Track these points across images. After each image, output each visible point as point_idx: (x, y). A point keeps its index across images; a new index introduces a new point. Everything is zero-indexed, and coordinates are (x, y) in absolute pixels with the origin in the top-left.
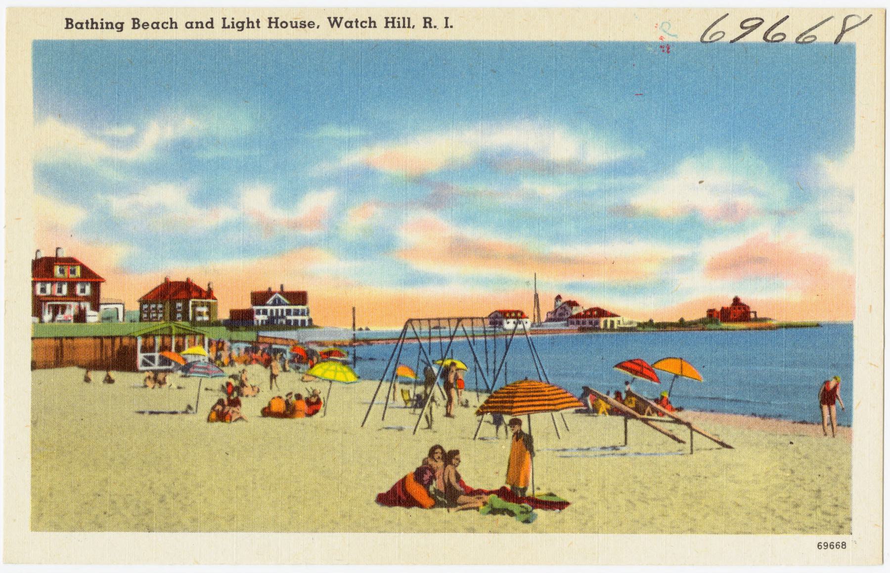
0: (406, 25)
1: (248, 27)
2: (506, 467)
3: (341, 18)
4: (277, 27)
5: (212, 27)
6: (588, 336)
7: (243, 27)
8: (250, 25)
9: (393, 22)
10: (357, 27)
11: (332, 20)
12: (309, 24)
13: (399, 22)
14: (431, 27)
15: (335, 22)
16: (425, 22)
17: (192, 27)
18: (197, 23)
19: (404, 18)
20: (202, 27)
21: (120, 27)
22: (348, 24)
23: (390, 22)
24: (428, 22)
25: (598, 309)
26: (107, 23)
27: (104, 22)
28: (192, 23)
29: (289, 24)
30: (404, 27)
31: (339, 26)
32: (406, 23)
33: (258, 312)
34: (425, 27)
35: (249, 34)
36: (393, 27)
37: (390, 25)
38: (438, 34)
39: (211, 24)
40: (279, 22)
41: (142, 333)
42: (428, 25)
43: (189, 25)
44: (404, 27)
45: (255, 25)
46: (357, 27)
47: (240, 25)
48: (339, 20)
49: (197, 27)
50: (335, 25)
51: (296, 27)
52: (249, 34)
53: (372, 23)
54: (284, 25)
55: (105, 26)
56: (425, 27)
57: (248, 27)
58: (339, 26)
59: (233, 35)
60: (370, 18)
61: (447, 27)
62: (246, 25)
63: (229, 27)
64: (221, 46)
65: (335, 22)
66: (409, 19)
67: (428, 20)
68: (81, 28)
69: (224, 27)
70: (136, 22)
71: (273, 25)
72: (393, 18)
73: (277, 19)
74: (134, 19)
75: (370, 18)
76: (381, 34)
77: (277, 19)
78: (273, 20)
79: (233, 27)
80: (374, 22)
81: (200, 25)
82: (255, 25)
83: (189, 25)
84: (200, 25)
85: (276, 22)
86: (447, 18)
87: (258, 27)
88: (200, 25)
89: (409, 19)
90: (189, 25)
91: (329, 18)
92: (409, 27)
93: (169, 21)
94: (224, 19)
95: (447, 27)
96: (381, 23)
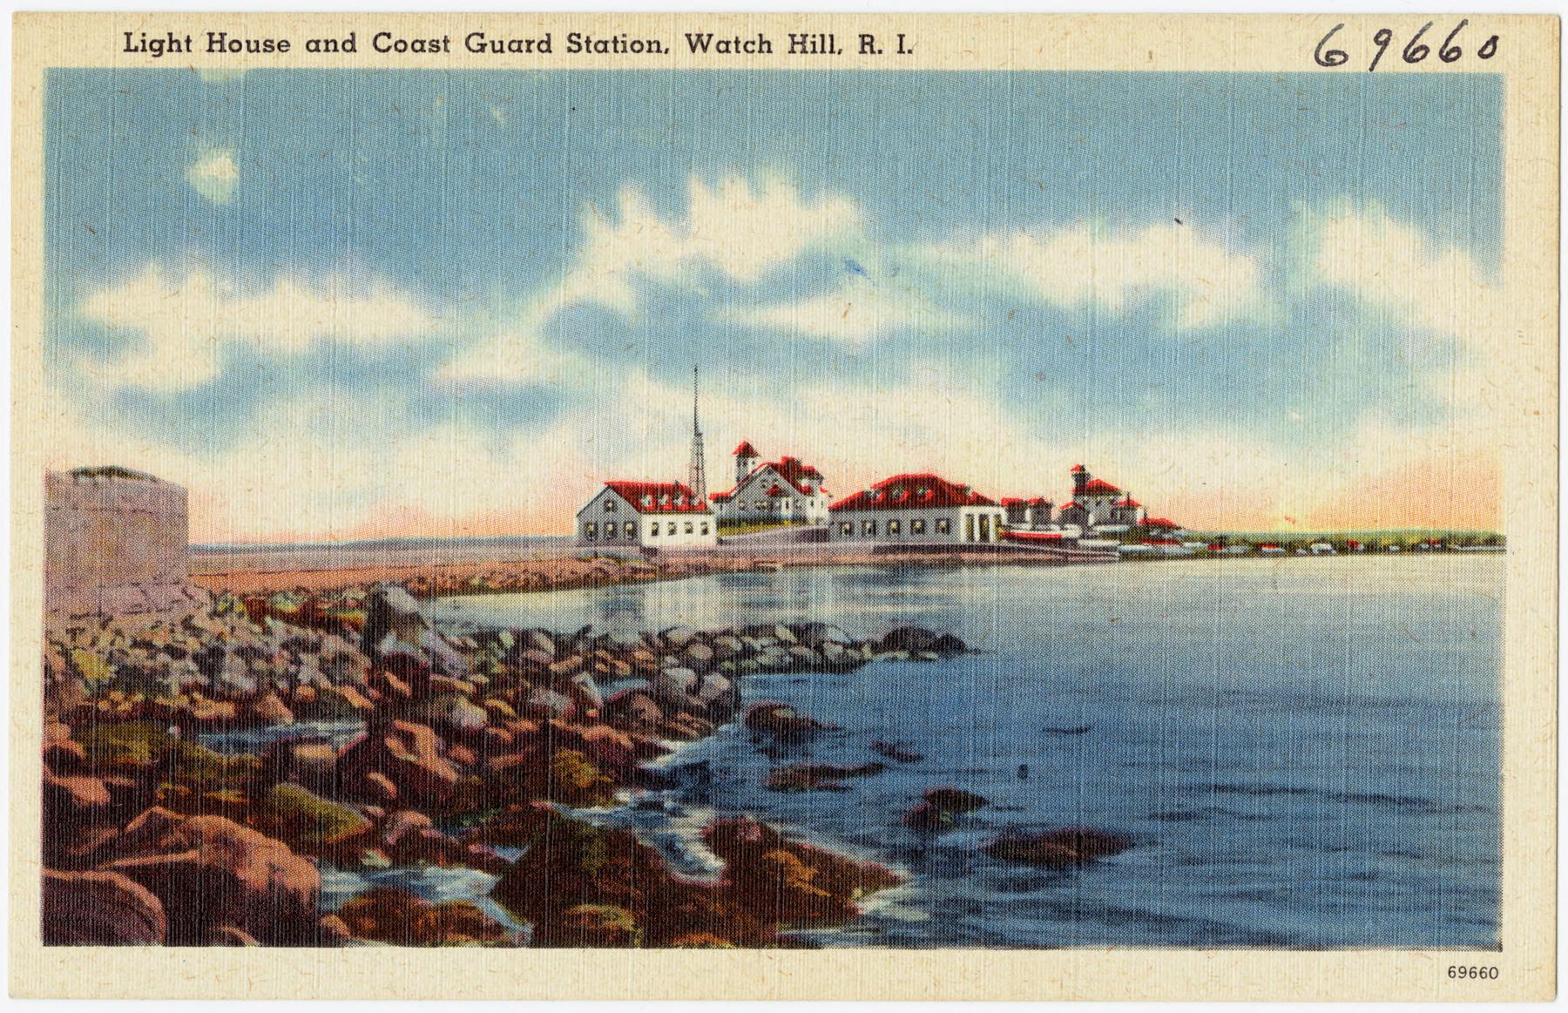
0: (827, 48)
1: (170, 50)
3: (710, 36)
5: (353, 49)
6: (1337, 523)
7: (161, 49)
8: (175, 46)
11: (694, 39)
15: (697, 43)
16: (863, 44)
17: (317, 50)
18: (327, 42)
20: (336, 50)
23: (798, 43)
24: (867, 43)
25: (932, 481)
28: (317, 42)
31: (705, 49)
32: (828, 44)
34: (863, 52)
36: (804, 51)
38: (888, 61)
39: (546, 45)
42: (867, 48)
43: (313, 46)
44: (823, 51)
45: (184, 46)
47: (156, 46)
48: (705, 39)
49: (327, 50)
52: (170, 61)
53: (765, 45)
54: (401, 46)
56: (863, 52)
57: (170, 50)
58: (705, 49)
59: (143, 60)
60: (170, 34)
61: (901, 51)
62: (166, 46)
63: (136, 49)
64: (299, 77)
65: (697, 43)
68: (605, 50)
70: (867, 43)
71: (216, 47)
72: (805, 36)
74: (862, 37)
75: (170, 34)
76: (780, 60)
78: (216, 37)
79: (144, 50)
81: (331, 46)
82: (184, 46)
83: (313, 46)
84: (331, 45)
85: (221, 42)
86: (901, 36)
88: (331, 45)
90: (312, 46)
91: (688, 36)
94: (128, 35)
95: (901, 51)
96: (781, 44)
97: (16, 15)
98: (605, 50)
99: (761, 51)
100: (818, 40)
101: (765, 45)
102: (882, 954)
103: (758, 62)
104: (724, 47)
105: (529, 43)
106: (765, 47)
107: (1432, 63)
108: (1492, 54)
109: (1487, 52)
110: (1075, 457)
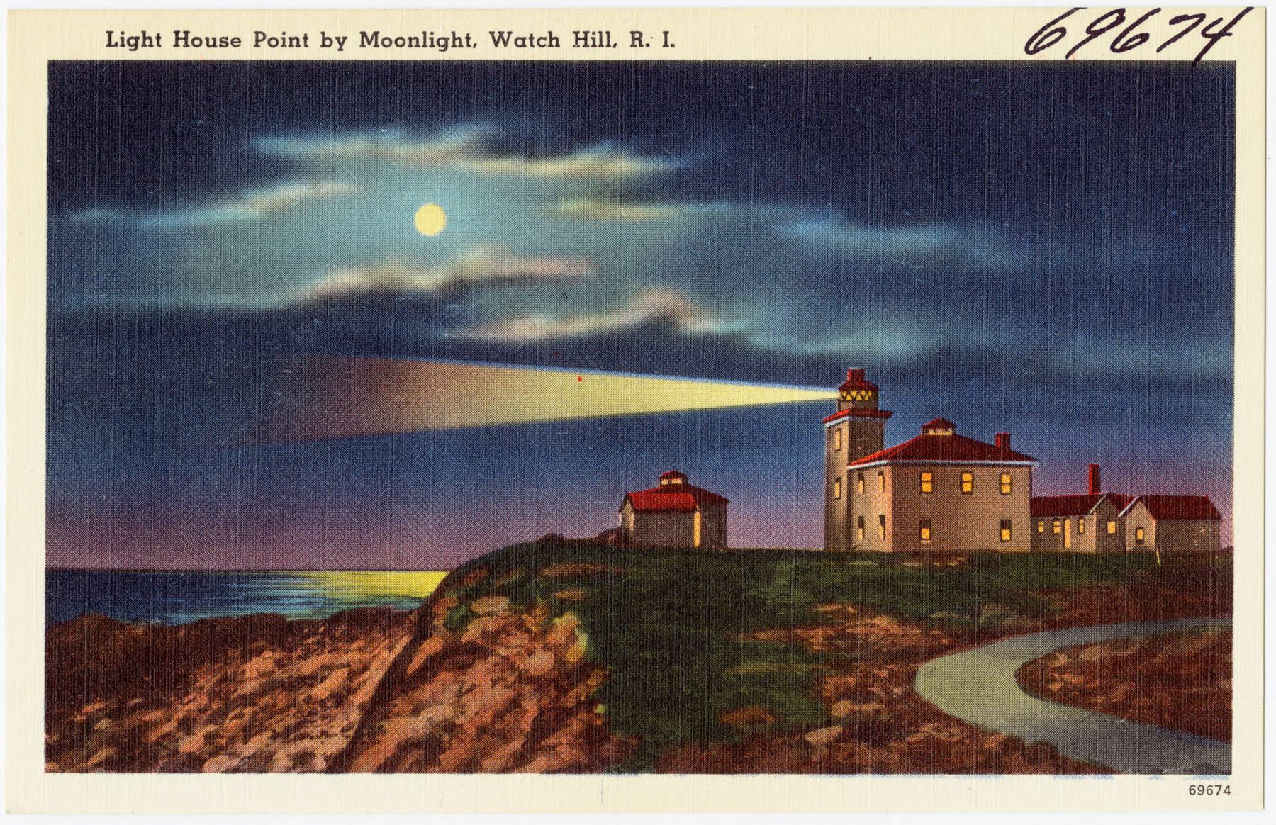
0: (605, 43)
2: (388, 573)
3: (510, 33)
4: (186, 45)
7: (446, 46)
9: (585, 39)
10: (532, 46)
12: (232, 42)
13: (594, 39)
14: (641, 45)
16: (634, 39)
22: (520, 42)
26: (291, 39)
27: (287, 37)
29: (204, 42)
30: (601, 45)
31: (505, 44)
35: (143, 54)
36: (586, 45)
37: (581, 43)
40: (190, 37)
42: (637, 43)
45: (155, 42)
46: (532, 46)
47: (132, 42)
48: (505, 36)
49: (291, 45)
50: (501, 43)
51: (214, 45)
55: (287, 42)
58: (505, 44)
60: (550, 33)
61: (666, 45)
62: (450, 42)
63: (116, 45)
65: (500, 39)
66: (608, 33)
67: (637, 36)
68: (524, 45)
69: (109, 45)
70: (259, 38)
71: (181, 42)
72: (586, 33)
73: (187, 33)
74: (633, 33)
75: (550, 33)
77: (187, 33)
78: (182, 35)
79: (123, 45)
80: (557, 39)
81: (294, 42)
82: (155, 42)
85: (186, 38)
86: (666, 33)
87: (159, 45)
89: (608, 33)
92: (608, 46)
93: (547, 36)
94: (110, 33)
97: (10, 11)
98: (524, 45)
99: (551, 45)
100: (597, 36)
101: (553, 40)
104: (521, 43)
106: (554, 42)
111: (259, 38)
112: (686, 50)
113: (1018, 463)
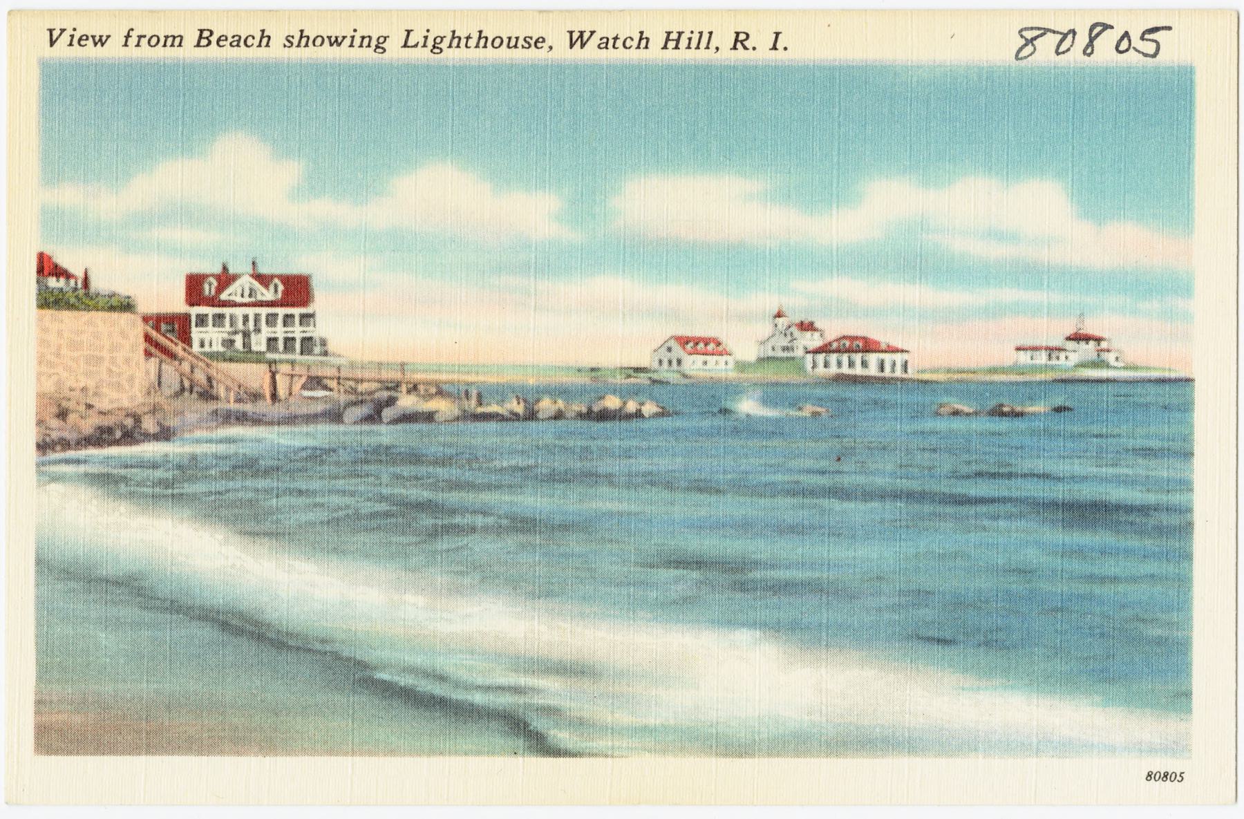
9: (678, 41)
11: (575, 36)
19: (701, 33)
21: (176, 40)
23: (672, 40)
31: (583, 45)
32: (704, 39)
33: (202, 320)
38: (760, 52)
41: (433, 426)
48: (586, 36)
63: (416, 46)
64: (189, 69)
65: (579, 39)
66: (711, 33)
67: (742, 37)
78: (674, 36)
82: (463, 42)
86: (777, 34)
95: (405, 46)
100: (695, 37)
102: (724, 762)
103: (703, 55)
105: (616, 38)
107: (1075, 55)
108: (1092, 52)
109: (1089, 51)
110: (771, 303)
111: (204, 37)
112: (805, 48)
113: (964, 376)
